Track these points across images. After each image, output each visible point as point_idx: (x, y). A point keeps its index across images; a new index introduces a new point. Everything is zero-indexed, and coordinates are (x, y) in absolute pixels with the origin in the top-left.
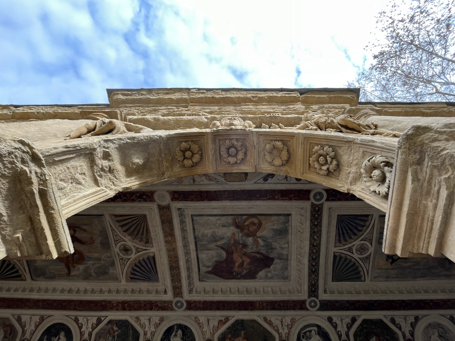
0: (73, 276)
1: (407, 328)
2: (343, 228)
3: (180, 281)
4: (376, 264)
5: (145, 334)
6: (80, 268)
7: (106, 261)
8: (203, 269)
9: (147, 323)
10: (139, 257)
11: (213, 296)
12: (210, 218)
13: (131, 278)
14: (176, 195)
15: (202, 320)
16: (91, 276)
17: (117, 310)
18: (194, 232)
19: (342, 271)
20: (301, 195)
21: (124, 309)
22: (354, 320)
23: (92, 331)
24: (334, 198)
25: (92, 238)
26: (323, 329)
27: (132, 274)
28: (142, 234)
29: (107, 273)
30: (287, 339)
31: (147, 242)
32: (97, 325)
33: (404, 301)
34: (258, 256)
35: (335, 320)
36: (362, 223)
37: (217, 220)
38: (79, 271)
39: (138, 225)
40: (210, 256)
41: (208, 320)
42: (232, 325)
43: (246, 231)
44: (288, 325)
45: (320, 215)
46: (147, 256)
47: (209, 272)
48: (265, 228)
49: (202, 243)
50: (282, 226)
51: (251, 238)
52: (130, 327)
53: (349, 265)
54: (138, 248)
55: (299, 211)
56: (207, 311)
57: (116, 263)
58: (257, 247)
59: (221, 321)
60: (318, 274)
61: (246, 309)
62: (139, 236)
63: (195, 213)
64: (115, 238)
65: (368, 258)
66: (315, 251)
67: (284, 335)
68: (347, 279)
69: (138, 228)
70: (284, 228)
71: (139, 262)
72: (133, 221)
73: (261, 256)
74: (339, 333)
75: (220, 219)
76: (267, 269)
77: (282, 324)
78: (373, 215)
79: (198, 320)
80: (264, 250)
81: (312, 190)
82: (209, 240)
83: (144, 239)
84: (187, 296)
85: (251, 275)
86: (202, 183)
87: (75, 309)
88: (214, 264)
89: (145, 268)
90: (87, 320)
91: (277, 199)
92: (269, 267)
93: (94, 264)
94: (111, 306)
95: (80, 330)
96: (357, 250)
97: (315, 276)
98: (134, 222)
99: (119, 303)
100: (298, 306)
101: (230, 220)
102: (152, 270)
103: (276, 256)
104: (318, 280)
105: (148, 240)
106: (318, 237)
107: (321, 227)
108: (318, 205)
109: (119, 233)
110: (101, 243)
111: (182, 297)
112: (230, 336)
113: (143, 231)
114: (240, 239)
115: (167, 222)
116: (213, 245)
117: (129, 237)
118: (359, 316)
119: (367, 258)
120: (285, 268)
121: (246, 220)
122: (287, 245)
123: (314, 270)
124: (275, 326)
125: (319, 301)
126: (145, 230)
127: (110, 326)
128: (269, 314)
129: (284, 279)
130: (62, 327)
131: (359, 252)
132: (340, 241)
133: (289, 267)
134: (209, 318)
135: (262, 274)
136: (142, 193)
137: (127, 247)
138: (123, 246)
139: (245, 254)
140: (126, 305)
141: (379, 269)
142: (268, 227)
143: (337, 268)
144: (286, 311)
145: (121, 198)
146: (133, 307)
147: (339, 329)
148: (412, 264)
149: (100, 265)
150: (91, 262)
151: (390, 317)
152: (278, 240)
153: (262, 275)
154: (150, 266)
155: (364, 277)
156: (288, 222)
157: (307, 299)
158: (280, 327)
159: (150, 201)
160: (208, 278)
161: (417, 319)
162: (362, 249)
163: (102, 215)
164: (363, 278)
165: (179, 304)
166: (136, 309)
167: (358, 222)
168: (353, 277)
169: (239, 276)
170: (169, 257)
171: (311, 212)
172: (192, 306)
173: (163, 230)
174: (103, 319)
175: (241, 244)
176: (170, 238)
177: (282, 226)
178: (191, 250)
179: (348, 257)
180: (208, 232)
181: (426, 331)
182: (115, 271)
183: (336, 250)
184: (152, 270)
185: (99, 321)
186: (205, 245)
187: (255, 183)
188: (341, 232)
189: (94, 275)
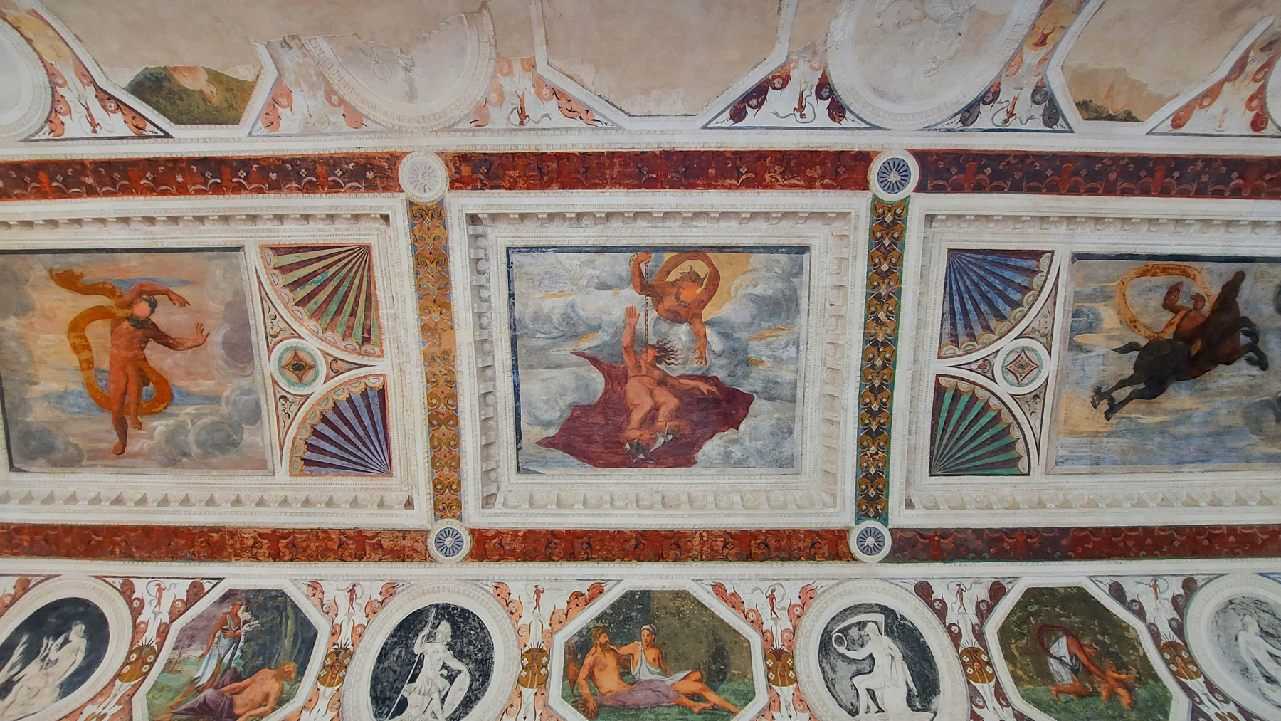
0: (134, 455)
1: (1161, 615)
2: (966, 296)
3: (456, 463)
4: (1062, 417)
5: (335, 632)
6: (155, 428)
7: (235, 404)
8: (533, 433)
9: (343, 600)
10: (335, 389)
11: (558, 515)
12: (562, 257)
13: (308, 462)
14: (466, 170)
15: (520, 591)
16: (185, 455)
17: (255, 558)
18: (512, 306)
19: (959, 439)
20: (841, 170)
21: (276, 556)
22: (997, 591)
23: (172, 622)
24: (941, 182)
25: (200, 328)
26: (903, 618)
27: (311, 448)
28: (353, 313)
29: (235, 445)
30: (789, 647)
31: (366, 340)
32: (188, 604)
33: (1148, 531)
34: (704, 387)
35: (938, 591)
36: (1021, 280)
37: (583, 264)
38: (152, 438)
39: (342, 281)
40: (561, 387)
41: (538, 593)
42: (613, 606)
43: (669, 302)
44: (791, 607)
45: (898, 241)
46: (362, 388)
47: (549, 443)
48: (729, 292)
49: (534, 342)
50: (779, 285)
51: (685, 328)
52: (290, 612)
53: (984, 421)
54: (336, 360)
55: (831, 229)
56: (536, 564)
57: (264, 413)
58: (702, 358)
59: (578, 595)
60: (888, 441)
61: (659, 557)
62: (344, 318)
65: (1038, 396)
66: (879, 362)
67: (777, 637)
68: (992, 466)
69: (342, 291)
70: (788, 293)
71: (336, 409)
73: (713, 389)
74: (954, 628)
75: (592, 262)
76: (730, 434)
77: (773, 606)
78: (1052, 252)
80: (721, 367)
81: (877, 153)
82: (556, 333)
83: (358, 331)
84: (475, 516)
85: (680, 454)
86: (545, 124)
87: (127, 555)
88: (568, 414)
89: (351, 428)
90: (160, 590)
91: (772, 187)
92: (736, 426)
93: (198, 416)
94: (238, 546)
95: (134, 619)
96: (1006, 369)
97: (880, 448)
99: (261, 535)
100: (825, 550)
101: (621, 264)
102: (372, 434)
103: (759, 386)
104: (886, 462)
105: (369, 331)
106: (889, 314)
107: (899, 281)
108: (894, 205)
109: (283, 303)
110: (227, 344)
111: (460, 518)
112: (603, 639)
113: (356, 302)
114: (650, 329)
115: (431, 259)
116: (564, 352)
117: (313, 323)
118: (1014, 578)
119: (1036, 397)
120: (785, 430)
121: (675, 263)
122: (792, 351)
123: (874, 427)
124: (751, 610)
125: (891, 530)
127: (227, 608)
128: (733, 573)
129: (781, 466)
130: (82, 609)
131: (1011, 377)
132: (955, 342)
133: (797, 429)
135: (712, 448)
136: (362, 161)
137: (301, 355)
138: (290, 354)
139: (663, 382)
140: (284, 542)
141: (1072, 433)
142: (737, 290)
143: (944, 430)
144: (787, 564)
145: (299, 179)
146: (305, 550)
147: (951, 617)
148: (1168, 418)
149: (216, 418)
150: (190, 409)
151: (1108, 581)
152: (767, 333)
153: (714, 453)
154: (367, 421)
155: (1026, 459)
156: (798, 274)
157: (853, 524)
158: (765, 612)
159: (386, 188)
160: (545, 463)
161: (1190, 585)
162: (1021, 367)
163: (237, 249)
164: (1023, 464)
165: (449, 541)
167: (1008, 274)
168: (994, 459)
169: (642, 456)
170: (430, 381)
171: (872, 232)
172: (487, 546)
173: (418, 287)
174: (207, 586)
175: (654, 347)
176: (436, 317)
177: (779, 285)
178: (498, 365)
179: (980, 393)
180: (554, 306)
181: (1220, 621)
182: (258, 439)
183: (943, 367)
184: (372, 434)
185: (196, 592)
186: (543, 348)
187: (705, 127)
188: (957, 305)
189: (195, 450)
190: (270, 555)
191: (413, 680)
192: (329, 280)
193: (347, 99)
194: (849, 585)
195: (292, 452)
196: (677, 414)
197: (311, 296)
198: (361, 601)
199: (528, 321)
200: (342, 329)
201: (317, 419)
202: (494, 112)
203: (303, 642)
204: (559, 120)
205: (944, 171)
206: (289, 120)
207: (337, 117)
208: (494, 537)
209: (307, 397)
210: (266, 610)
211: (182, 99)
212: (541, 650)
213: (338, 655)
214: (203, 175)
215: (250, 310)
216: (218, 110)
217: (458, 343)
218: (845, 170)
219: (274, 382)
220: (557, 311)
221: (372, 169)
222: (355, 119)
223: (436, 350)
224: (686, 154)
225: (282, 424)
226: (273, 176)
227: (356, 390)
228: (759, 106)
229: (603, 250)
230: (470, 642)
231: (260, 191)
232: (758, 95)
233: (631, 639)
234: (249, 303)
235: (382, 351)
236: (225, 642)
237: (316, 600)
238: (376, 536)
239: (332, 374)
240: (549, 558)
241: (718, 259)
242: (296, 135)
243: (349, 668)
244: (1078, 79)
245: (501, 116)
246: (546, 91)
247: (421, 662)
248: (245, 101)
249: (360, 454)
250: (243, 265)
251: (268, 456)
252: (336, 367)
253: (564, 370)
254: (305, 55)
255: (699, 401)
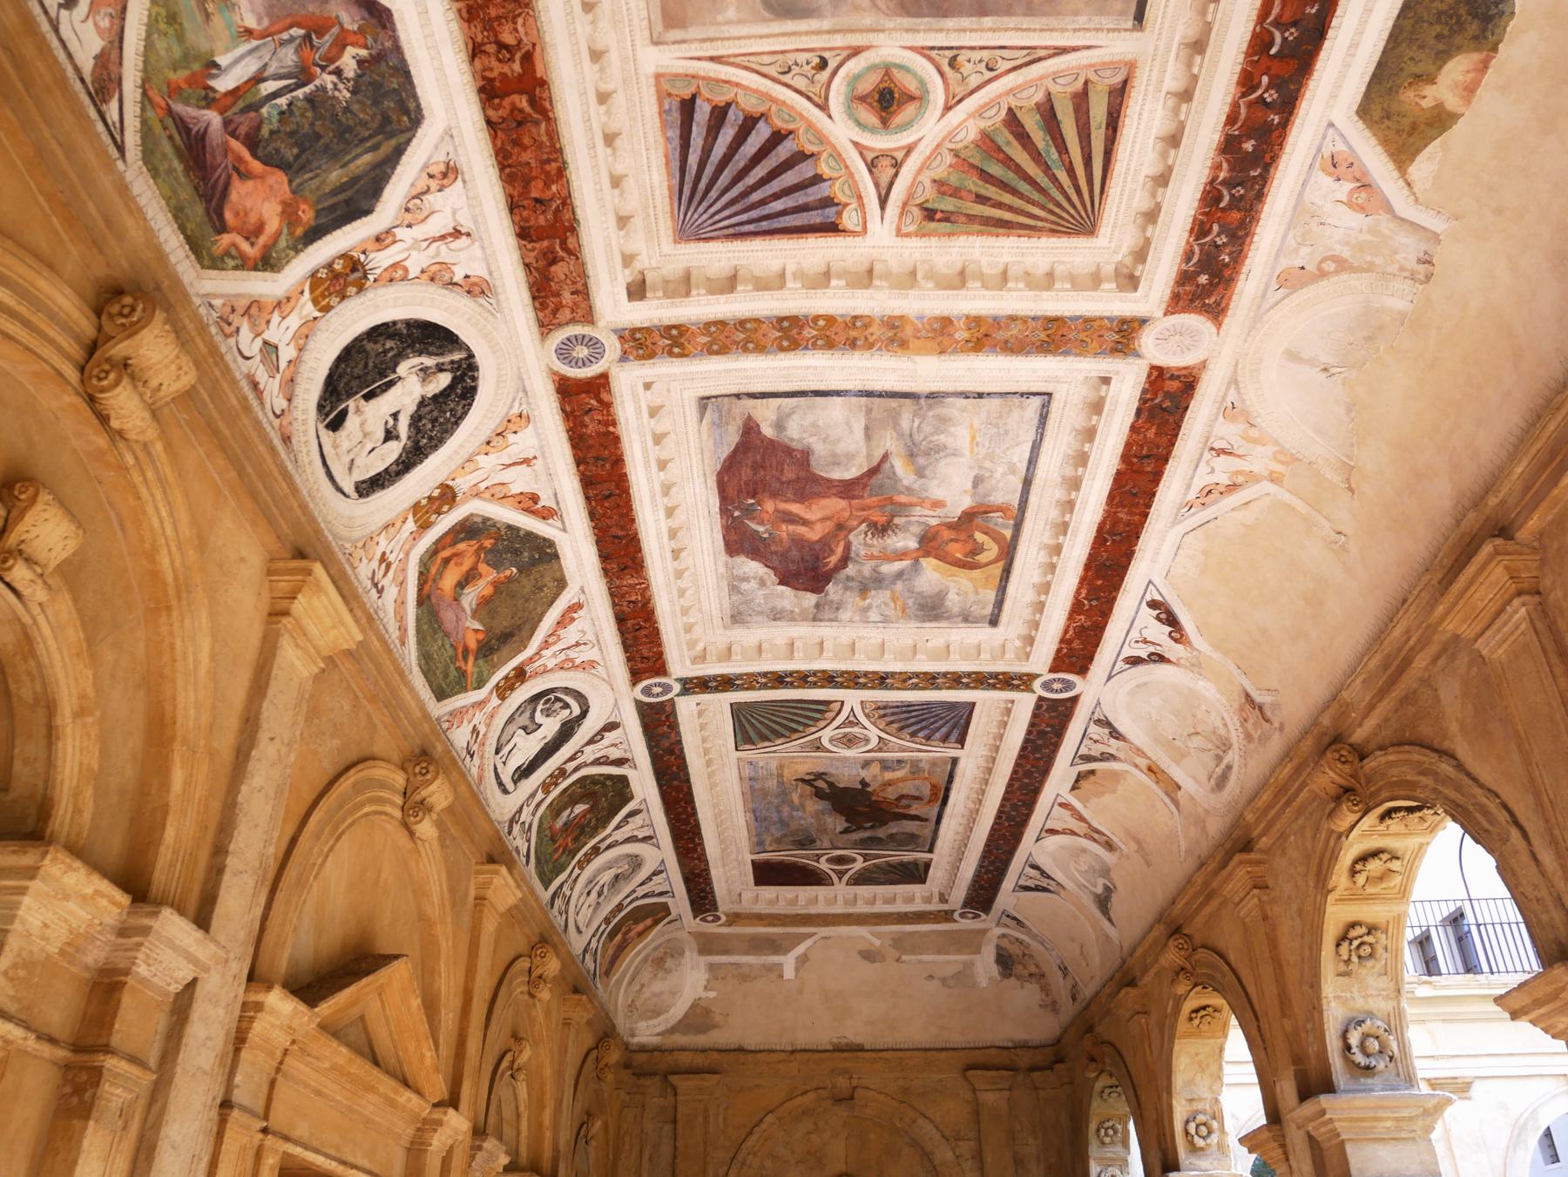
10: (837, 156)
12: (1027, 447)
13: (688, 107)
15: (522, 442)
17: (475, 51)
21: (489, 92)
28: (981, 199)
31: (930, 214)
34: (833, 560)
41: (526, 461)
42: (529, 534)
44: (572, 660)
46: (841, 198)
51: (913, 544)
52: (387, 148)
54: (897, 165)
57: (790, 25)
58: (872, 557)
59: (535, 498)
62: (973, 184)
63: (1055, 406)
64: (976, 55)
68: (742, 727)
69: (1024, 187)
72: (1071, 171)
73: (831, 566)
79: (513, 427)
82: (917, 438)
83: (948, 204)
86: (1203, 468)
94: (493, 12)
98: (1062, 176)
99: (528, 58)
101: (1005, 491)
102: (754, 214)
105: (947, 220)
109: (1019, 88)
111: (624, 358)
112: (488, 543)
113: (999, 205)
117: (971, 133)
120: (777, 616)
126: (1008, 216)
128: (599, 619)
134: (538, 464)
136: (1227, 273)
137: (910, 110)
138: (912, 86)
140: (523, 102)
145: (1229, 184)
146: (517, 142)
163: (1139, 17)
166: (503, 158)
173: (1013, 318)
175: (890, 521)
176: (962, 335)
182: (731, 13)
190: (490, 81)
191: (368, 397)
192: (1047, 170)
193: (1324, 283)
194: (605, 686)
195: (707, 79)
196: (799, 542)
197: (1023, 137)
198: (444, 252)
199: (939, 410)
200: (954, 180)
201: (779, 124)
202: (1240, 427)
203: (347, 202)
204: (1202, 479)
205: (1051, 721)
206: (1329, 192)
207: (1304, 257)
208: (600, 401)
209: (824, 107)
210: (376, 102)
211: (1439, 37)
212: (454, 496)
213: (354, 270)
214: (1294, 24)
215: (1011, 21)
216: (1392, 91)
217: (918, 359)
218: (1077, 653)
219: (856, 52)
220: (951, 440)
221: (1211, 283)
222: (1291, 280)
223: (908, 331)
224: (1126, 568)
225: (766, 59)
226: (1248, 146)
227: (838, 191)
228: (1158, 618)
229: (1027, 483)
230: (436, 420)
231: (1231, 119)
232: (1171, 620)
233: (496, 565)
234: (1026, 22)
235: (908, 235)
236: (289, 57)
237: (424, 182)
238: (570, 252)
239: (870, 156)
240: (579, 462)
241: (997, 570)
242: (1301, 194)
243: (346, 303)
244: (1116, 777)
245: (1228, 433)
246: (1240, 479)
247: (391, 384)
248: (1385, 142)
249: (713, 194)
250: (1108, 22)
251: (694, 32)
252: (885, 166)
253: (862, 443)
254: (1402, 269)
255: (817, 558)
